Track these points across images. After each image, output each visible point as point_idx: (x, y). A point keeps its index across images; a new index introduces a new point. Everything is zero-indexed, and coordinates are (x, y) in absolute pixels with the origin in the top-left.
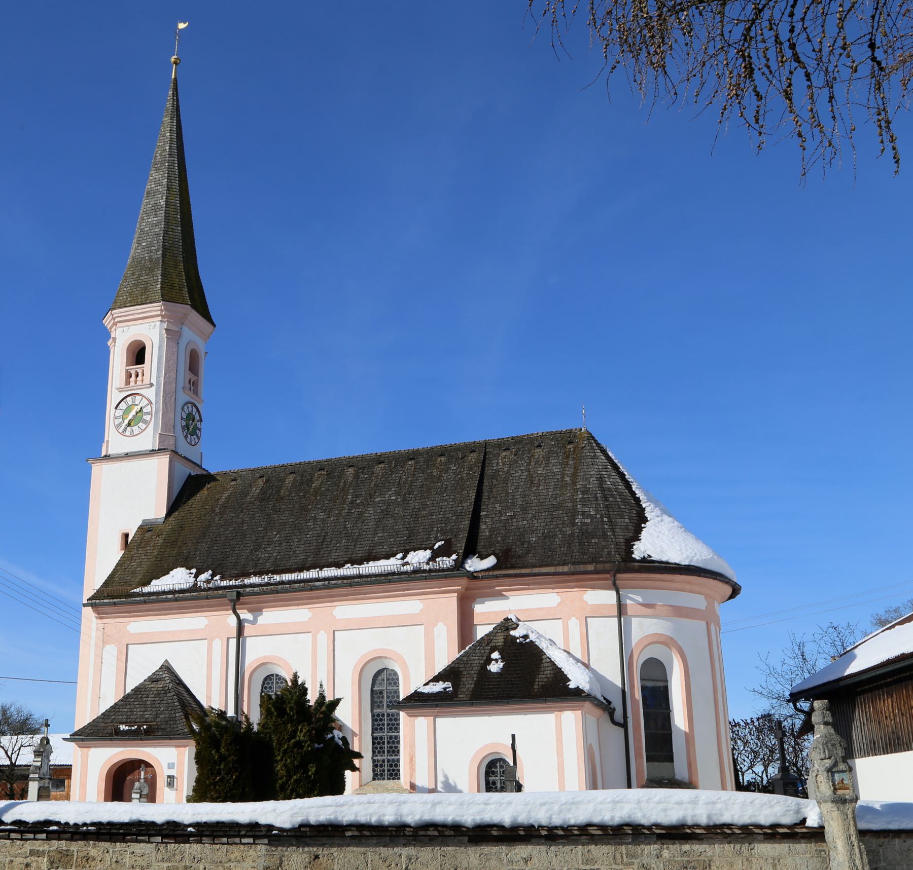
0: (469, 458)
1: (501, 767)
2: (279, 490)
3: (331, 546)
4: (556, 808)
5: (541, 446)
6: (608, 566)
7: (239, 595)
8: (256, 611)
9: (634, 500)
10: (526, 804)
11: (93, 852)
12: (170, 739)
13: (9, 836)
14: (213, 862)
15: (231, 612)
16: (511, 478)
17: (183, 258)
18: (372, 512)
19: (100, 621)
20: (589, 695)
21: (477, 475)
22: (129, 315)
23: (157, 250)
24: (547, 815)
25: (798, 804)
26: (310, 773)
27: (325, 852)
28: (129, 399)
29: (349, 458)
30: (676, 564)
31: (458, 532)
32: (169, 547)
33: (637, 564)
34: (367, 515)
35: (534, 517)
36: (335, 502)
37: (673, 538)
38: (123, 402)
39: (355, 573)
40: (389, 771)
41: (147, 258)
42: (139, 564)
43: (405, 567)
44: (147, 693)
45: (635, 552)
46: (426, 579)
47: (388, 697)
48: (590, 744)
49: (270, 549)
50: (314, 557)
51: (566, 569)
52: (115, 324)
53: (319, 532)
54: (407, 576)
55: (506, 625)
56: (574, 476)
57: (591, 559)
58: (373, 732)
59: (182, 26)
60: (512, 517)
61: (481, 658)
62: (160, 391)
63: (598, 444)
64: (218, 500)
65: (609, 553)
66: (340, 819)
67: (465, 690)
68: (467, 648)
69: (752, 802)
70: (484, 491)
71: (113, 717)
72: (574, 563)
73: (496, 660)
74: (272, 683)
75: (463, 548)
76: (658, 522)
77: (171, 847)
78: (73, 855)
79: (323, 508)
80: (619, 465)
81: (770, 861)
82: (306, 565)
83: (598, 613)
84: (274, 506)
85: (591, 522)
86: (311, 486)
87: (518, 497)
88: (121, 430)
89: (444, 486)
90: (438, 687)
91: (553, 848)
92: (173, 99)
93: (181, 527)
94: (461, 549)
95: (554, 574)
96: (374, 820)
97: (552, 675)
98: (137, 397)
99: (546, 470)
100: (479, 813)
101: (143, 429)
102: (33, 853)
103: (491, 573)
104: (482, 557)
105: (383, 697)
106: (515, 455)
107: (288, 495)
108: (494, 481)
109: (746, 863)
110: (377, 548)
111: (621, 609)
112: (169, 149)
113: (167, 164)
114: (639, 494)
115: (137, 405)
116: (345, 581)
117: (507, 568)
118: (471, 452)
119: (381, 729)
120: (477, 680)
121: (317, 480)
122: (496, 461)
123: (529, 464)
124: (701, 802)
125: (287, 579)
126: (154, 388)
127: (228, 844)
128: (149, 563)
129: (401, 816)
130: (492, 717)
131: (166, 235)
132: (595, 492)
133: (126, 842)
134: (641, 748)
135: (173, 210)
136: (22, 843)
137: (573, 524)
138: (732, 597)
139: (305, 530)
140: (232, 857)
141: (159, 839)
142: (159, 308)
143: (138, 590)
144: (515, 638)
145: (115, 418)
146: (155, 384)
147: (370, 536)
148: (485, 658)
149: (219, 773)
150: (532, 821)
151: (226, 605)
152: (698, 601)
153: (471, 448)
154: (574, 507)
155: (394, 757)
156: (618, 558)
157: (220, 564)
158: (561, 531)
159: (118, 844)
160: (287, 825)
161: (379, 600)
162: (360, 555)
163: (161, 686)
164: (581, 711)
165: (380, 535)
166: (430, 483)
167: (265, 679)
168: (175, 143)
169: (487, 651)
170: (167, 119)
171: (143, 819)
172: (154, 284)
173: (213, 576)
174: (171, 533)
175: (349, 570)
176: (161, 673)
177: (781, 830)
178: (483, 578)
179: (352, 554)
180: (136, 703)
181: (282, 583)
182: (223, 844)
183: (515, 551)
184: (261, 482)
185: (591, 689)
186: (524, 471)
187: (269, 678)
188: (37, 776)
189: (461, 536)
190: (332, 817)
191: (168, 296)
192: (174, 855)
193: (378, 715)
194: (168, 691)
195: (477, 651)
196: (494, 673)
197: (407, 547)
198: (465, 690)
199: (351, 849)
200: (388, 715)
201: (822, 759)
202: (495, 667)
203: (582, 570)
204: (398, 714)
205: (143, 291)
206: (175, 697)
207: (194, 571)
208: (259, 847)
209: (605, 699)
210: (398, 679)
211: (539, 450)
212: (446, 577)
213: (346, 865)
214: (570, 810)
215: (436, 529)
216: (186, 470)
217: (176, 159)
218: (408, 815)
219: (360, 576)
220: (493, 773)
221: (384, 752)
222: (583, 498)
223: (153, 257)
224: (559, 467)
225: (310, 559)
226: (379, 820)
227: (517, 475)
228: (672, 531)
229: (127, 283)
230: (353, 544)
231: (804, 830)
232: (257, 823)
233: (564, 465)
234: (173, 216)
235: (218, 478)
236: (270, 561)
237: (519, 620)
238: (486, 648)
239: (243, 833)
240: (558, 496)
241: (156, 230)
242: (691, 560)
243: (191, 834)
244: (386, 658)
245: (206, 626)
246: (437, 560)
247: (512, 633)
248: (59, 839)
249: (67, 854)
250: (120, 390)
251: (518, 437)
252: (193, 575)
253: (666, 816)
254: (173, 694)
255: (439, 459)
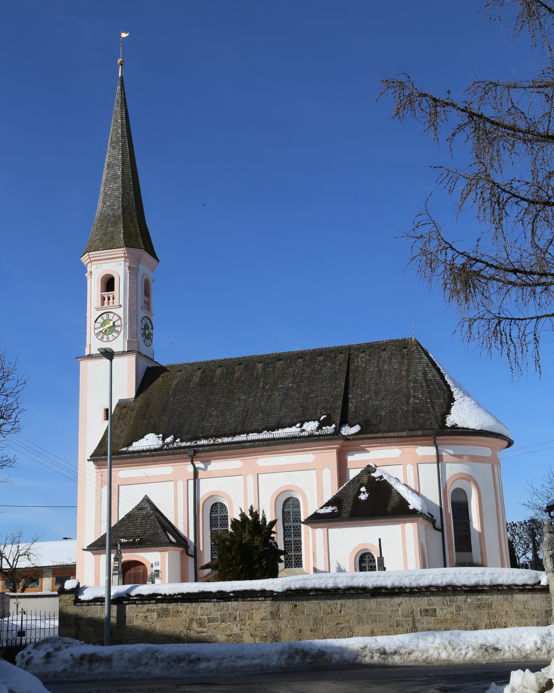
0: (339, 358)
1: (369, 557)
2: (213, 379)
3: (252, 418)
4: (413, 578)
5: (386, 350)
6: (431, 432)
7: (195, 452)
8: (207, 462)
9: (446, 387)
10: (399, 576)
11: (181, 608)
12: (157, 547)
13: (135, 602)
14: (244, 610)
15: (190, 463)
16: (367, 372)
17: (136, 214)
18: (277, 395)
19: (98, 470)
20: (421, 513)
21: (345, 369)
22: (117, 254)
23: (118, 209)
24: (409, 582)
25: (536, 574)
26: (263, 565)
27: (300, 603)
28: (104, 316)
29: (258, 356)
30: (472, 429)
31: (335, 409)
32: (141, 419)
33: (448, 430)
34: (274, 397)
35: (383, 399)
36: (252, 387)
37: (471, 412)
38: (100, 318)
39: (271, 437)
40: (295, 562)
41: (111, 214)
42: (121, 431)
43: (303, 433)
44: (136, 517)
45: (448, 422)
46: (317, 441)
47: (293, 515)
48: (422, 543)
49: (211, 420)
50: (242, 426)
51: (404, 434)
52: (91, 262)
53: (243, 408)
54: (304, 439)
55: (368, 470)
56: (408, 371)
57: (420, 427)
58: (284, 538)
59: (124, 35)
60: (369, 399)
61: (354, 491)
62: (126, 310)
63: (423, 349)
64: (171, 385)
65: (431, 423)
66: (306, 586)
67: (346, 511)
68: (345, 485)
69: (513, 573)
70: (350, 380)
71: (115, 534)
72: (409, 430)
73: (364, 493)
74: (217, 508)
75: (339, 420)
76: (462, 402)
77: (222, 604)
78: (170, 611)
79: (244, 392)
80: (436, 362)
81: (522, 603)
82: (237, 432)
83: (425, 460)
84: (210, 390)
85: (420, 402)
86: (234, 376)
87: (372, 385)
88: (100, 337)
89: (324, 377)
90: (329, 510)
91: (412, 598)
92: (121, 92)
93: (147, 405)
94: (338, 421)
95: (398, 437)
96: (323, 586)
97: (398, 501)
98: (110, 314)
99: (390, 367)
100: (375, 581)
101: (116, 336)
102: (148, 610)
103: (358, 437)
104: (351, 426)
105: (290, 516)
106: (369, 356)
107: (219, 383)
108: (356, 374)
109: (509, 604)
110: (282, 419)
111: (439, 458)
112: (121, 132)
113: (120, 144)
114: (449, 382)
115: (111, 320)
116: (265, 443)
117: (367, 433)
118: (340, 353)
119: (289, 536)
120: (353, 505)
121: (238, 372)
122: (357, 360)
123: (378, 362)
124: (487, 574)
125: (226, 441)
126: (122, 308)
127: (251, 601)
128: (129, 430)
129: (336, 584)
130: (363, 528)
131: (124, 198)
132: (421, 382)
133: (198, 603)
134: (452, 544)
135: (127, 178)
136: (142, 606)
137: (408, 404)
138: (508, 447)
139: (234, 407)
140: (254, 607)
141: (216, 600)
142: (123, 252)
143: (123, 449)
144: (375, 478)
145: (95, 329)
146: (122, 305)
147: (277, 411)
148: (356, 491)
149: (232, 566)
150: (401, 585)
151: (187, 458)
152: (486, 452)
153: (339, 350)
154: (409, 392)
155: (298, 553)
156: (437, 426)
157: (178, 431)
158: (400, 408)
159: (194, 604)
160: (280, 591)
161: (286, 454)
162: (272, 424)
163: (145, 512)
164: (416, 523)
165: (284, 411)
166: (314, 375)
167: (213, 506)
168: (125, 127)
169: (357, 486)
170: (118, 108)
171: (205, 590)
172: (118, 234)
173: (175, 439)
174: (141, 408)
175: (265, 435)
176: (143, 504)
177: (527, 587)
178: (353, 440)
179: (267, 424)
180: (129, 524)
181: (223, 444)
182: (249, 601)
183: (372, 421)
184: (199, 373)
185: (422, 509)
186: (375, 367)
187: (215, 505)
188: (117, 572)
189: (337, 412)
190: (302, 586)
191: (129, 243)
192: (223, 608)
193: (287, 527)
194: (150, 516)
195: (351, 487)
196: (363, 500)
197: (303, 419)
198: (346, 511)
199: (313, 601)
200: (294, 527)
201: (548, 551)
202: (363, 497)
203: (415, 434)
204: (300, 526)
205: (111, 239)
206: (155, 519)
207: (161, 435)
208: (267, 602)
209: (429, 513)
210: (299, 504)
211: (385, 353)
212: (330, 439)
213: (311, 609)
214: (420, 579)
215: (320, 407)
216: (146, 364)
217: (127, 140)
218: (340, 584)
219: (274, 439)
220: (364, 561)
221: (291, 550)
222: (414, 386)
223: (116, 214)
224: (398, 365)
225: (239, 427)
226: (326, 587)
227: (371, 370)
228: (470, 408)
229: (98, 233)
230: (267, 417)
231: (539, 587)
232: (265, 590)
233: (401, 363)
234: (127, 183)
235: (168, 369)
236: (212, 428)
237: (377, 467)
238: (357, 484)
239: (259, 595)
240: (398, 384)
241: (116, 194)
242: (482, 427)
243: (232, 597)
244: (292, 490)
245: (172, 472)
246: (324, 428)
247: (373, 475)
248: (162, 603)
249: (167, 610)
250: (98, 309)
251: (370, 343)
252: (161, 439)
253: (469, 581)
254: (154, 517)
255: (319, 358)
